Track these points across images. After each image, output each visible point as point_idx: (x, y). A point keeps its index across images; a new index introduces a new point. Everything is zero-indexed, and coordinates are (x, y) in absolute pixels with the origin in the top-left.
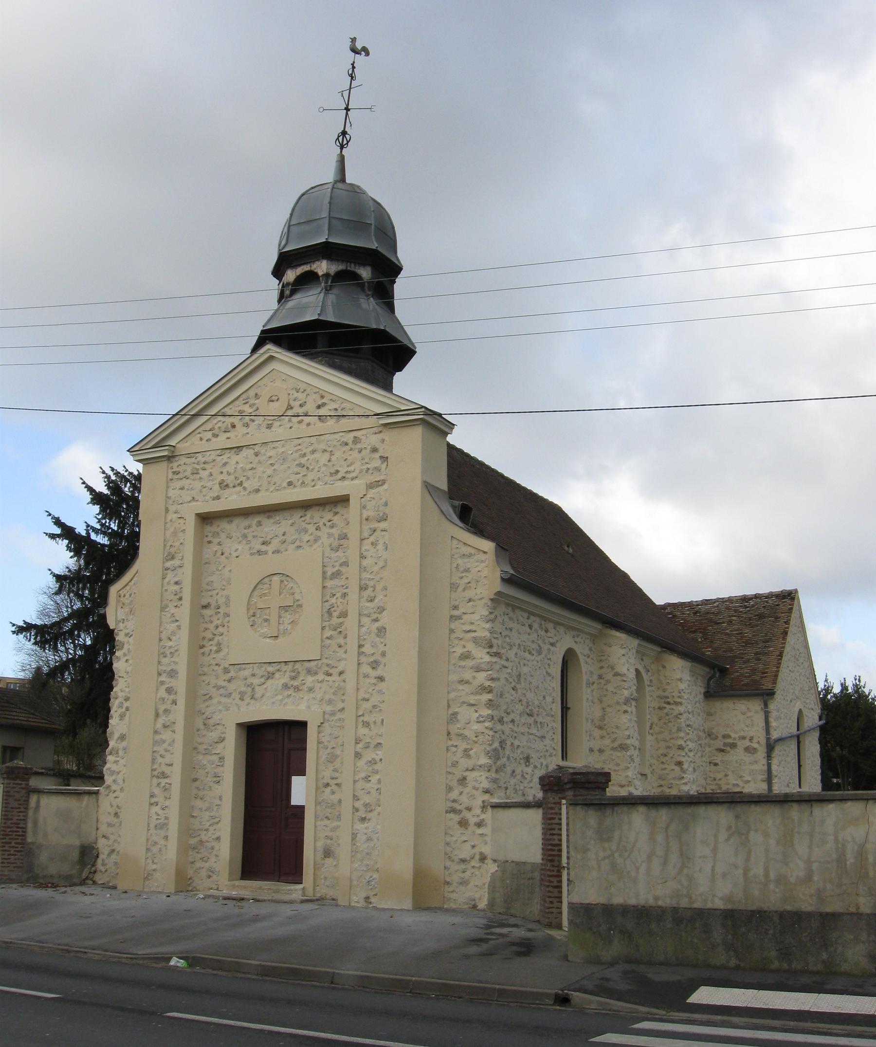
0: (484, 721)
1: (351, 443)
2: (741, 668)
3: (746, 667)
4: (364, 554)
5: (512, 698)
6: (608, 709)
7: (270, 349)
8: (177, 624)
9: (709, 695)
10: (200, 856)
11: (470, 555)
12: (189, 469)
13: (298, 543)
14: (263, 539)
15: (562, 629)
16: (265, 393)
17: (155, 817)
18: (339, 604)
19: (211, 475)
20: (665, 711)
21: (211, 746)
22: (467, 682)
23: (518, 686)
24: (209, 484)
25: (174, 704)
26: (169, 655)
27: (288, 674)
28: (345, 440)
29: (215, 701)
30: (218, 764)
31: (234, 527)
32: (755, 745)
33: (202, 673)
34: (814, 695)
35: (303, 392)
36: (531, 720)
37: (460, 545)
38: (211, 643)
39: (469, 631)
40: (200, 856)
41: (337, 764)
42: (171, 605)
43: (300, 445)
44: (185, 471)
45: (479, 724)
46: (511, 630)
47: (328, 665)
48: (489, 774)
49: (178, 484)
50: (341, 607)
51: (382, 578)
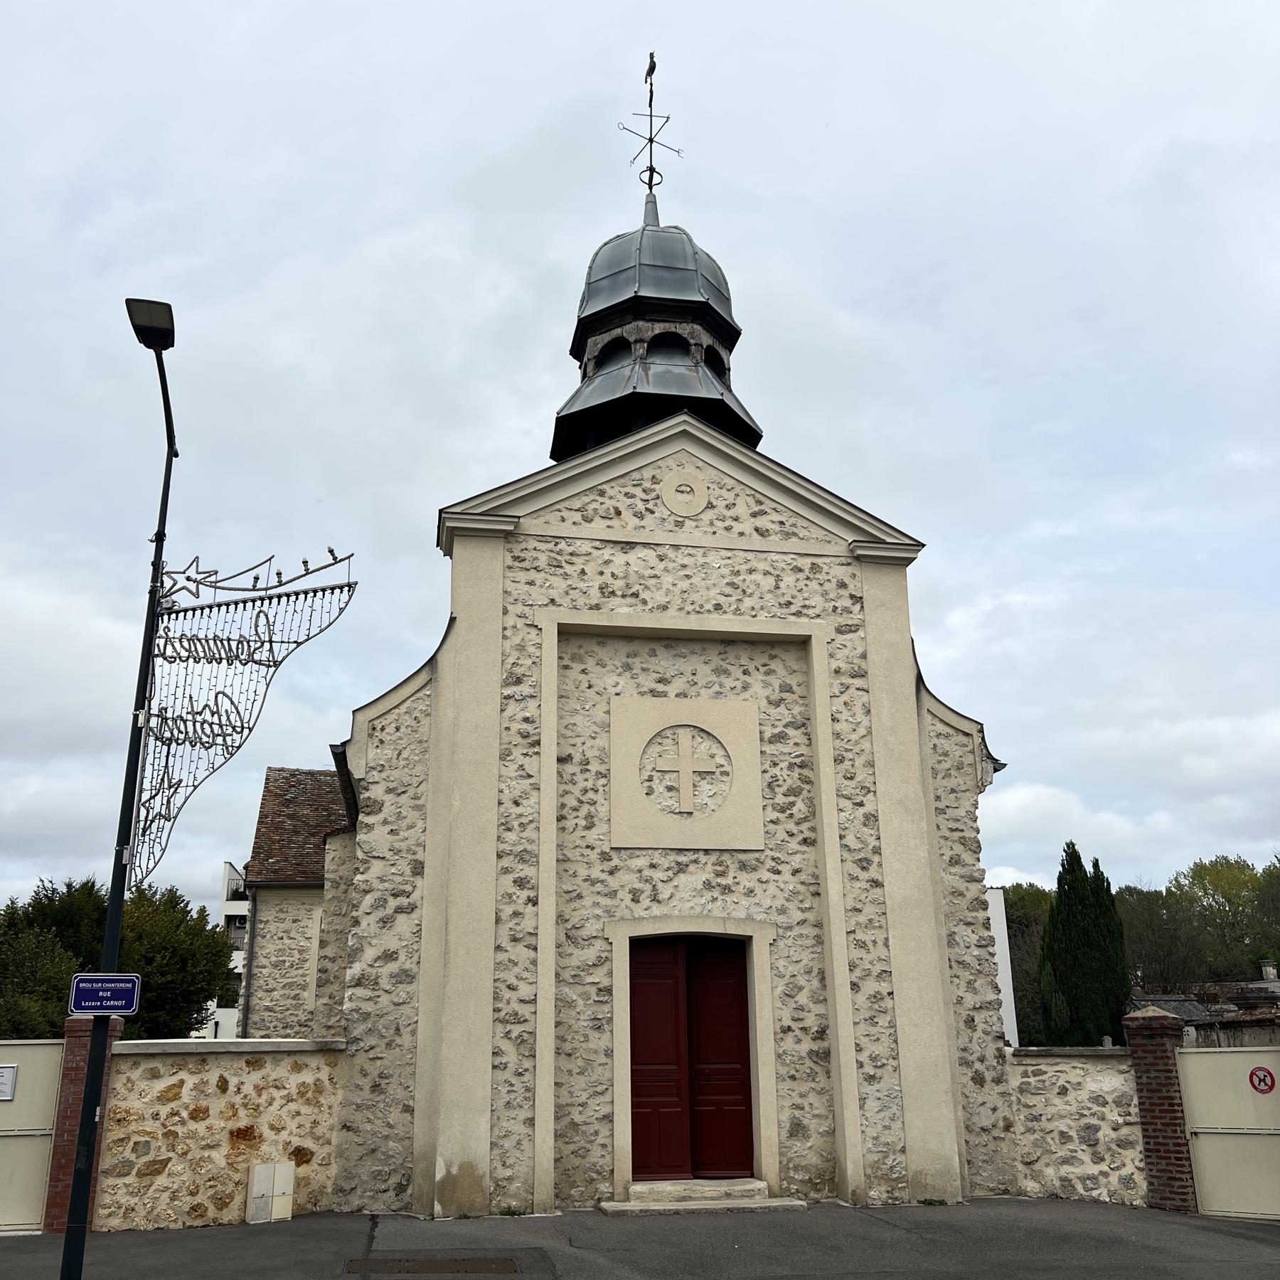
4: (837, 716)
10: (572, 1147)
13: (716, 688)
14: (660, 675)
18: (786, 777)
19: (583, 572)
22: (961, 894)
27: (709, 867)
29: (587, 901)
30: (597, 999)
35: (728, 490)
37: (936, 722)
39: (957, 830)
40: (572, 1147)
42: (517, 753)
43: (729, 558)
47: (773, 859)
49: (523, 576)
50: (789, 782)
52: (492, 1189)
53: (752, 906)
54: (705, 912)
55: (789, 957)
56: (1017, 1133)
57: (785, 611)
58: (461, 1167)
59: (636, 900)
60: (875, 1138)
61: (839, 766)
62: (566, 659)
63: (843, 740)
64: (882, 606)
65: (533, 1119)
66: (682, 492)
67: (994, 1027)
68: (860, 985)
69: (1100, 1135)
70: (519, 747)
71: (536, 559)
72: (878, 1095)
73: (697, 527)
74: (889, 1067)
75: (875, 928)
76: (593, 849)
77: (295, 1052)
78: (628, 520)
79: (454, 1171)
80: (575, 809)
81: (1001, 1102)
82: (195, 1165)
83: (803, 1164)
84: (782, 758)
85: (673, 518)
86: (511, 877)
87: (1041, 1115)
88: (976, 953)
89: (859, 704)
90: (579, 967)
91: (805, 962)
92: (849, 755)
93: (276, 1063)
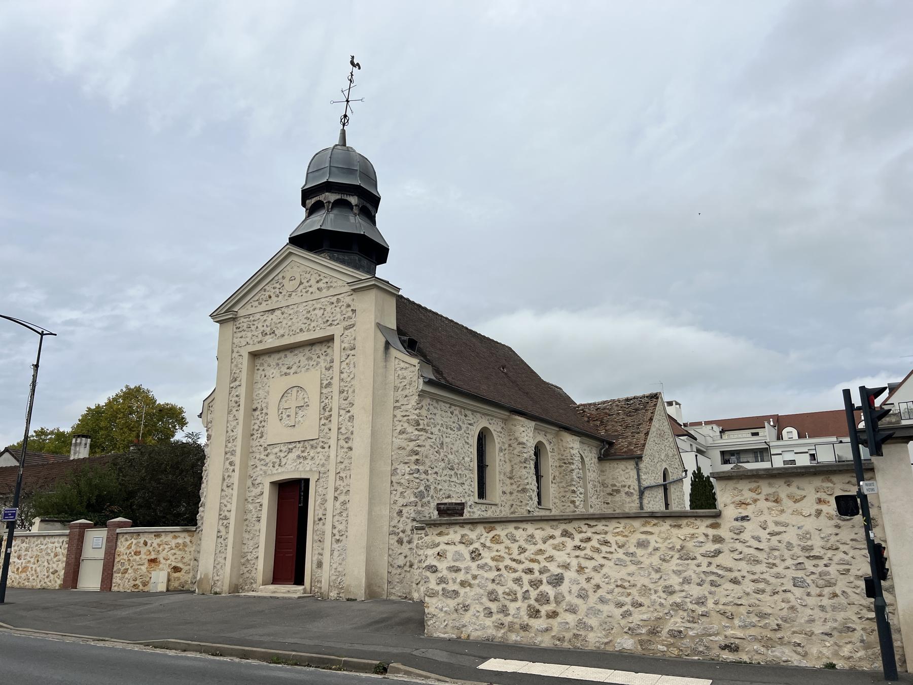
0: (413, 474)
2: (622, 442)
3: (626, 441)
5: (435, 458)
6: (515, 466)
8: (237, 421)
9: (600, 459)
10: (247, 569)
12: (245, 325)
13: (307, 367)
15: (478, 415)
19: (257, 327)
20: (563, 468)
22: (404, 448)
23: (441, 450)
24: (256, 333)
26: (232, 441)
28: (332, 301)
29: (258, 469)
31: (273, 360)
32: (632, 491)
34: (678, 459)
36: (452, 473)
37: (401, 362)
38: (257, 432)
42: (234, 410)
44: (243, 326)
46: (435, 414)
49: (239, 335)
60: (336, 569)
65: (226, 558)
72: (339, 549)
74: (345, 536)
76: (262, 446)
79: (202, 577)
80: (257, 430)
82: (135, 571)
85: (288, 293)
89: (352, 362)
93: (166, 535)
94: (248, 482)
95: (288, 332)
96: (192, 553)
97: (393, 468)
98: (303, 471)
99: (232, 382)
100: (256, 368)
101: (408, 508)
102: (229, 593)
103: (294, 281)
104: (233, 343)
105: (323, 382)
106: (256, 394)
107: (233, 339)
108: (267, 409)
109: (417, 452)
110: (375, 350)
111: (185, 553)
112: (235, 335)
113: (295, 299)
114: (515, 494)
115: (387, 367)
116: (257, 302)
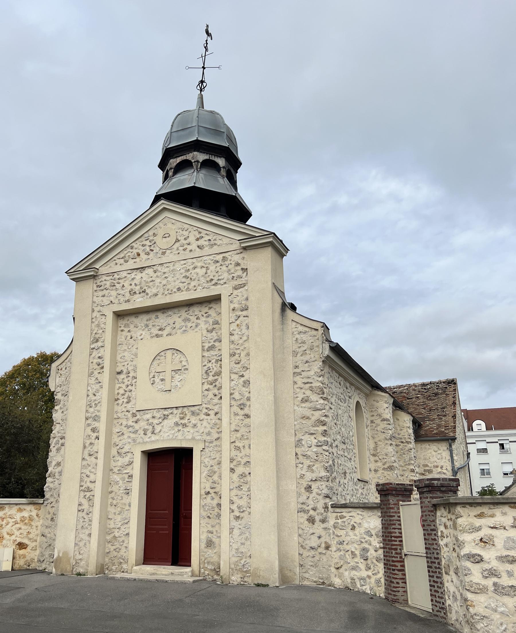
0: (321, 446)
1: (221, 261)
4: (232, 332)
6: (379, 443)
7: (163, 203)
8: (100, 384)
10: (114, 547)
11: (305, 333)
12: (108, 283)
13: (184, 328)
14: (160, 327)
16: (160, 232)
17: (82, 520)
18: (214, 367)
19: (123, 286)
20: (401, 447)
21: (123, 467)
22: (308, 418)
24: (122, 292)
25: (97, 439)
26: (94, 406)
27: (178, 416)
29: (125, 436)
33: (116, 417)
35: (186, 231)
37: (298, 325)
39: (308, 383)
41: (216, 477)
42: (96, 372)
43: (185, 264)
44: (106, 284)
45: (318, 448)
47: (206, 408)
48: (327, 483)
49: (101, 293)
50: (215, 369)
51: (245, 348)
52: (74, 563)
53: (195, 433)
54: (174, 438)
55: (210, 457)
56: (333, 551)
57: (210, 284)
58: (63, 554)
59: (145, 434)
60: (237, 549)
61: (233, 358)
62: (122, 327)
63: (235, 344)
64: (257, 270)
65: (90, 534)
66: (166, 237)
67: (323, 491)
68: (235, 469)
69: (369, 554)
70: (97, 370)
71: (106, 284)
72: (240, 527)
73: (171, 252)
74: (247, 512)
75: (245, 439)
76: (129, 412)
77: (20, 504)
78: (143, 257)
79: (61, 555)
80: (123, 395)
81: (324, 534)
83: (211, 561)
84: (212, 358)
85: (161, 251)
86: (90, 428)
87: (344, 541)
88: (315, 450)
89: (244, 324)
90: (121, 466)
91: (217, 459)
92: (238, 352)
93: (10, 508)
94: (112, 451)
95: (162, 291)
96: (39, 527)
97: (297, 439)
98: (183, 439)
99: (93, 343)
100: (120, 329)
101: (318, 483)
102: (96, 575)
103: (167, 238)
104: (94, 302)
105: (204, 344)
106: (121, 355)
107: (93, 298)
108: (135, 372)
109: (324, 422)
110: (273, 312)
111: (32, 528)
112: (96, 294)
113: (170, 257)
114: (381, 471)
115: (284, 330)
116: (123, 259)
